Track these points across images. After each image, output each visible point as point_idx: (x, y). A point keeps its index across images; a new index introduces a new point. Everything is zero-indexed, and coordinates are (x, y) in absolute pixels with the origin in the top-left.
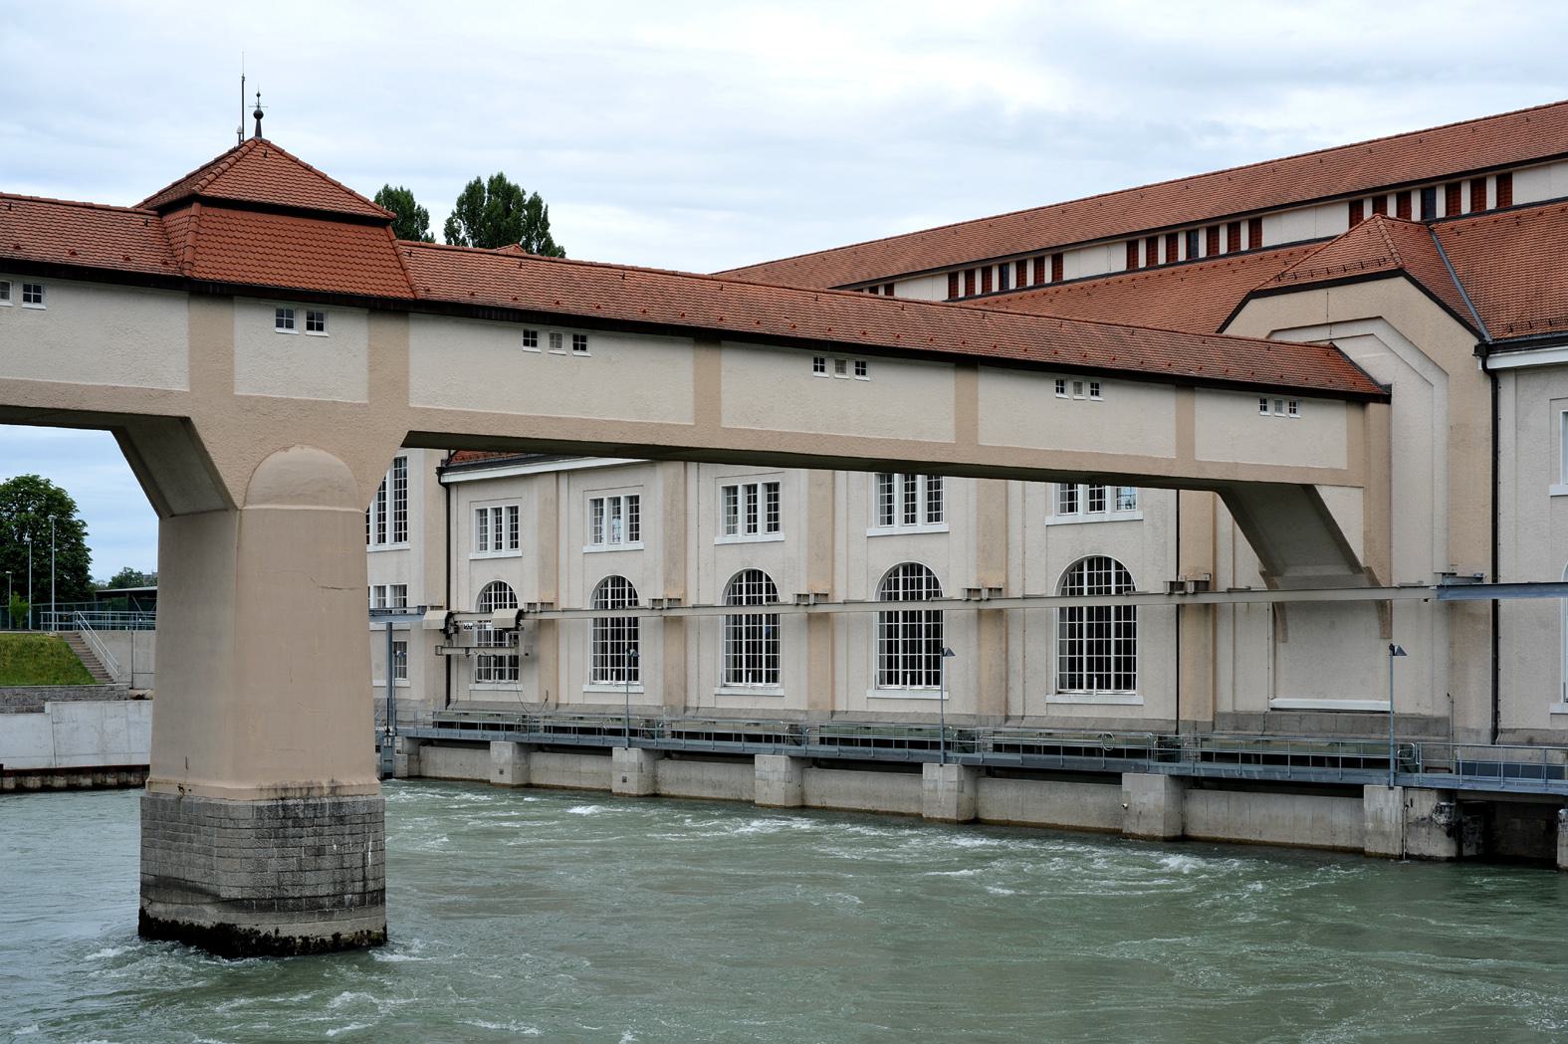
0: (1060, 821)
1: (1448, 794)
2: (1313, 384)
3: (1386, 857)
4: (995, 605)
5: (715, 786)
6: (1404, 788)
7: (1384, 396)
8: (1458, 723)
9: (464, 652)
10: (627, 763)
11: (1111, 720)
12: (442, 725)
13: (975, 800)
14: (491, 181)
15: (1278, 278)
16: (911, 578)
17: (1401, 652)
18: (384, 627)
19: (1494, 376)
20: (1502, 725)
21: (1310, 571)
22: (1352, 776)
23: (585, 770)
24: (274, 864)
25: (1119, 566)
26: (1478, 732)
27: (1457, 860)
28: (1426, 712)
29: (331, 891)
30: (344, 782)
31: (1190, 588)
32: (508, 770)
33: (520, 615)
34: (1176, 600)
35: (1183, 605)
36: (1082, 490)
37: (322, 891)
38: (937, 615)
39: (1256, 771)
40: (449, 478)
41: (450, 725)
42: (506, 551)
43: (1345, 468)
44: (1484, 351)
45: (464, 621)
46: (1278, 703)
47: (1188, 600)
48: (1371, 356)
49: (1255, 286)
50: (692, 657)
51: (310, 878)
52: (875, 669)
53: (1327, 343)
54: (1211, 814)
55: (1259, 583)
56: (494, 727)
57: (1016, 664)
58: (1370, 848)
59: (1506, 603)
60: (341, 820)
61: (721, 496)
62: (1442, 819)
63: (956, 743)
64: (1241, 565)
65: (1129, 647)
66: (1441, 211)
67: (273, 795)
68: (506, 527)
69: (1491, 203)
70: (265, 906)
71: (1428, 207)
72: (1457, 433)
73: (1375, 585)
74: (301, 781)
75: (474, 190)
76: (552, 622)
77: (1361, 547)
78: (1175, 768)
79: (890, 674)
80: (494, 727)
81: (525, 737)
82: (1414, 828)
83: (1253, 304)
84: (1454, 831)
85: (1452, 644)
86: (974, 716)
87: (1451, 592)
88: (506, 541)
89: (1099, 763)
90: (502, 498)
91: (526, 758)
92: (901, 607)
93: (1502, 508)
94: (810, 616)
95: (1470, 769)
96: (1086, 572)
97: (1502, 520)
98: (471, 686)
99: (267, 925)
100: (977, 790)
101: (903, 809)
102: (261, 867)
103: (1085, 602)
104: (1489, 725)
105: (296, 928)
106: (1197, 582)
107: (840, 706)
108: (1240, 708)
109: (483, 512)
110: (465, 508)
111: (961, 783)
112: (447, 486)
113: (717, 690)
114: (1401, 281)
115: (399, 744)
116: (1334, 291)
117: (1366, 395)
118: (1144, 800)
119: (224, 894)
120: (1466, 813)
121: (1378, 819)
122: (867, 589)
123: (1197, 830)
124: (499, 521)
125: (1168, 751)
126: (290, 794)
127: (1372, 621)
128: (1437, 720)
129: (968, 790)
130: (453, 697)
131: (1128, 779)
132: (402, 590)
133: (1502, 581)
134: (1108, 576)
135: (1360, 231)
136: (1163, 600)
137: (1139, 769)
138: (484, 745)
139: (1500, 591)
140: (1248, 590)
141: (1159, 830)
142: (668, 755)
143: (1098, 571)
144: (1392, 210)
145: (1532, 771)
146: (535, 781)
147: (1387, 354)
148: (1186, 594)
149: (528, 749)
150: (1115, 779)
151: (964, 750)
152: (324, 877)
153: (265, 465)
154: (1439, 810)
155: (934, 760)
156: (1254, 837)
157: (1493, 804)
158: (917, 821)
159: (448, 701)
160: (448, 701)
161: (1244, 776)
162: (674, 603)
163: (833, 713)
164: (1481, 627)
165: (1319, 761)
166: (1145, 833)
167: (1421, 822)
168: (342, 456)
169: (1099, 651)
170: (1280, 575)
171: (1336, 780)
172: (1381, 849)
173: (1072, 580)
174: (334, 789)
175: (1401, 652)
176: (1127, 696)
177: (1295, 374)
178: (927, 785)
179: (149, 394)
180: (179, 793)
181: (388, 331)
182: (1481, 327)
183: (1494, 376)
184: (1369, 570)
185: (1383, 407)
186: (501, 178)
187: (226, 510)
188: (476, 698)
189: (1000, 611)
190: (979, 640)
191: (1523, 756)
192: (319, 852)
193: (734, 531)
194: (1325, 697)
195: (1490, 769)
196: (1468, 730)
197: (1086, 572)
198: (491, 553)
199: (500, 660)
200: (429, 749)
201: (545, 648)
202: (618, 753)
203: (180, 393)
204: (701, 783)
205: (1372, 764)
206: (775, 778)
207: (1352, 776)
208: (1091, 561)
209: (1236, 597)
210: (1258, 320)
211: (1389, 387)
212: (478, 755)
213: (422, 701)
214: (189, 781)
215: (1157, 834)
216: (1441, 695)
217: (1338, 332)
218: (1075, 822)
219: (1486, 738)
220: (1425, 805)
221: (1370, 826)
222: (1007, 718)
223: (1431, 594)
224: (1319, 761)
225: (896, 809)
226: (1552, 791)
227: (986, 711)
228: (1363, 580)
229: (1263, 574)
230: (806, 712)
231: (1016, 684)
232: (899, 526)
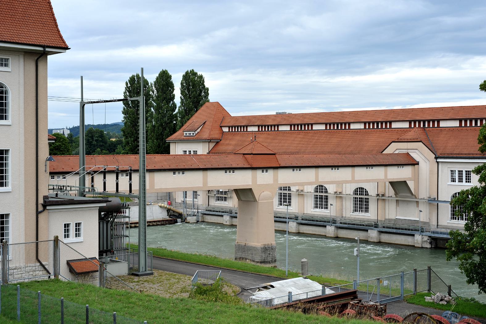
1: (430, 237)
3: (419, 247)
6: (422, 235)
8: (431, 223)
9: (214, 195)
13: (337, 233)
14: (190, 71)
15: (398, 139)
17: (421, 211)
19: (438, 162)
20: (439, 224)
21: (404, 194)
24: (264, 256)
25: (365, 189)
26: (434, 225)
27: (431, 248)
30: (272, 243)
34: (378, 198)
35: (379, 199)
37: (270, 260)
39: (394, 231)
43: (411, 177)
44: (436, 158)
46: (397, 217)
47: (380, 198)
48: (416, 156)
49: (393, 140)
51: (269, 258)
52: (313, 205)
53: (407, 153)
54: (385, 238)
55: (394, 196)
57: (344, 207)
60: (272, 249)
62: (429, 241)
66: (426, 126)
67: (263, 246)
71: (424, 125)
72: (431, 172)
74: (267, 243)
75: (187, 73)
77: (413, 191)
78: (379, 229)
79: (316, 206)
82: (424, 243)
83: (393, 143)
84: (431, 243)
85: (430, 209)
86: (335, 216)
87: (430, 201)
91: (232, 219)
93: (439, 186)
95: (434, 232)
97: (439, 188)
98: (214, 202)
100: (337, 231)
101: (321, 234)
104: (437, 224)
106: (382, 195)
107: (305, 212)
111: (335, 230)
113: (276, 207)
117: (415, 163)
118: (373, 235)
120: (432, 240)
121: (417, 240)
125: (376, 226)
126: (266, 245)
127: (415, 204)
128: (427, 223)
129: (336, 231)
130: (210, 204)
133: (439, 200)
134: (363, 191)
136: (375, 197)
137: (371, 229)
139: (439, 202)
147: (418, 156)
148: (380, 197)
152: (270, 258)
153: (261, 195)
154: (428, 239)
155: (329, 225)
156: (394, 242)
157: (437, 238)
159: (209, 205)
160: (209, 205)
161: (392, 232)
164: (435, 207)
165: (406, 229)
166: (373, 241)
167: (425, 241)
168: (270, 192)
170: (398, 194)
172: (418, 246)
175: (421, 211)
176: (367, 215)
178: (327, 230)
179: (247, 185)
180: (245, 244)
181: (276, 171)
183: (438, 162)
184: (415, 195)
185: (418, 165)
186: (193, 70)
187: (255, 201)
188: (216, 205)
190: (336, 202)
191: (443, 230)
194: (406, 217)
195: (437, 233)
196: (432, 225)
197: (358, 190)
200: (206, 215)
205: (416, 230)
206: (294, 226)
209: (389, 198)
211: (419, 162)
212: (219, 218)
213: (201, 204)
214: (247, 243)
215: (375, 241)
216: (428, 218)
217: (409, 151)
219: (436, 226)
220: (426, 238)
221: (416, 242)
223: (427, 201)
224: (406, 229)
225: (320, 234)
227: (338, 215)
228: (414, 197)
229: (395, 194)
230: (298, 213)
231: (344, 210)
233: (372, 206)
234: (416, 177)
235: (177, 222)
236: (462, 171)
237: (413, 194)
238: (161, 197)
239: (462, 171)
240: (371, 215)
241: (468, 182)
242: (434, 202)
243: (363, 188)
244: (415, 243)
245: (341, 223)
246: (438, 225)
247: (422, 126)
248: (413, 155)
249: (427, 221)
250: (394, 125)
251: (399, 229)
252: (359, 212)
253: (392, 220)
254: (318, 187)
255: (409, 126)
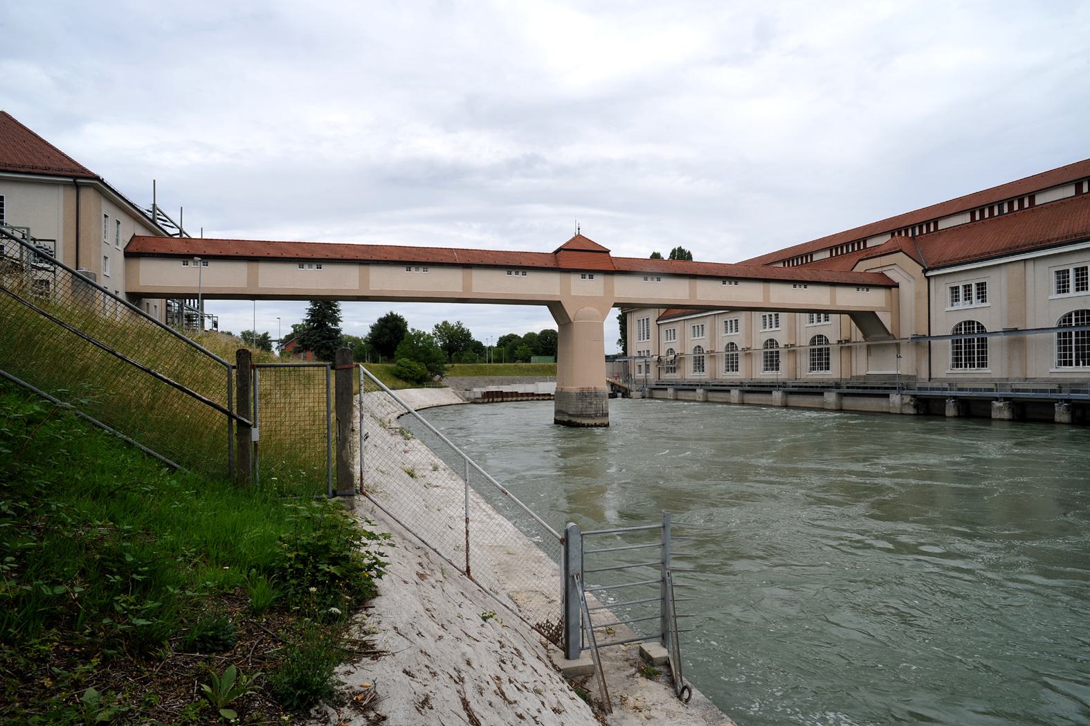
0: (808, 406)
2: (874, 283)
3: (896, 414)
4: (793, 349)
5: (722, 398)
7: (897, 286)
8: (919, 377)
10: (777, 396)
11: (823, 379)
12: (657, 385)
15: (867, 255)
16: (771, 342)
18: (644, 360)
19: (928, 278)
20: (932, 377)
21: (876, 336)
22: (886, 392)
23: (690, 395)
24: (580, 406)
25: (978, 323)
27: (917, 414)
28: (910, 374)
29: (594, 413)
31: (843, 342)
32: (701, 397)
33: (675, 356)
34: (840, 345)
36: (822, 315)
37: (592, 413)
38: (828, 349)
39: (860, 391)
40: (659, 322)
41: (659, 385)
42: (734, 333)
44: (925, 271)
45: (663, 358)
46: (869, 373)
47: (843, 345)
48: (893, 275)
50: (717, 366)
51: (589, 410)
56: (731, 386)
57: (798, 365)
58: (891, 411)
59: (933, 342)
61: (692, 328)
62: (912, 403)
63: (739, 385)
64: (857, 335)
65: (828, 359)
68: (735, 325)
69: (932, 230)
70: (579, 416)
71: (913, 233)
72: (918, 296)
73: (895, 339)
75: (674, 251)
76: (683, 358)
78: (838, 391)
80: (731, 386)
81: (676, 387)
84: (915, 406)
85: (917, 355)
88: (672, 338)
89: (818, 390)
90: (671, 327)
92: (769, 350)
94: (789, 351)
96: (963, 327)
97: (931, 319)
99: (579, 421)
102: (577, 407)
103: (816, 347)
104: (928, 377)
105: (586, 421)
108: (858, 374)
109: (726, 322)
110: (663, 329)
112: (659, 325)
114: (901, 253)
115: (646, 389)
116: (882, 257)
117: (891, 285)
119: (570, 413)
121: (893, 403)
122: (761, 346)
123: (845, 408)
124: (771, 319)
127: (894, 349)
131: (825, 394)
132: (648, 351)
133: (932, 335)
135: (894, 238)
138: (666, 389)
140: (860, 342)
141: (834, 407)
142: (711, 391)
143: (820, 338)
144: (903, 234)
145: (938, 389)
146: (679, 398)
149: (744, 392)
150: (822, 394)
151: (784, 387)
154: (911, 401)
155: (776, 390)
158: (771, 406)
162: (712, 352)
163: (752, 379)
167: (906, 404)
169: (970, 354)
171: (882, 393)
173: (813, 341)
174: (595, 388)
176: (828, 372)
177: (868, 281)
178: (774, 397)
182: (925, 265)
183: (928, 278)
185: (897, 289)
188: (666, 378)
189: (794, 350)
191: (935, 385)
192: (591, 404)
193: (772, 327)
195: (926, 389)
197: (963, 327)
198: (669, 341)
199: (671, 368)
201: (682, 365)
202: (698, 390)
203: (356, 290)
204: (718, 398)
207: (886, 392)
208: (818, 336)
209: (855, 344)
210: (862, 267)
218: (812, 406)
219: (927, 380)
220: (907, 399)
221: (891, 405)
222: (796, 379)
226: (944, 394)
229: (863, 337)
231: (798, 370)
232: (768, 329)
233: (834, 359)
234: (895, 308)
235: (616, 397)
236: (970, 286)
237: (890, 332)
238: (618, 373)
239: (970, 286)
240: (832, 373)
241: (1083, 289)
242: (923, 342)
243: (973, 322)
244: (890, 407)
245: (848, 388)
246: (930, 379)
247: (910, 235)
248: (889, 274)
249: (913, 374)
250: (942, 225)
251: (725, 386)
252: (966, 366)
253: (861, 376)
254: (961, 325)
255: (1076, 193)
